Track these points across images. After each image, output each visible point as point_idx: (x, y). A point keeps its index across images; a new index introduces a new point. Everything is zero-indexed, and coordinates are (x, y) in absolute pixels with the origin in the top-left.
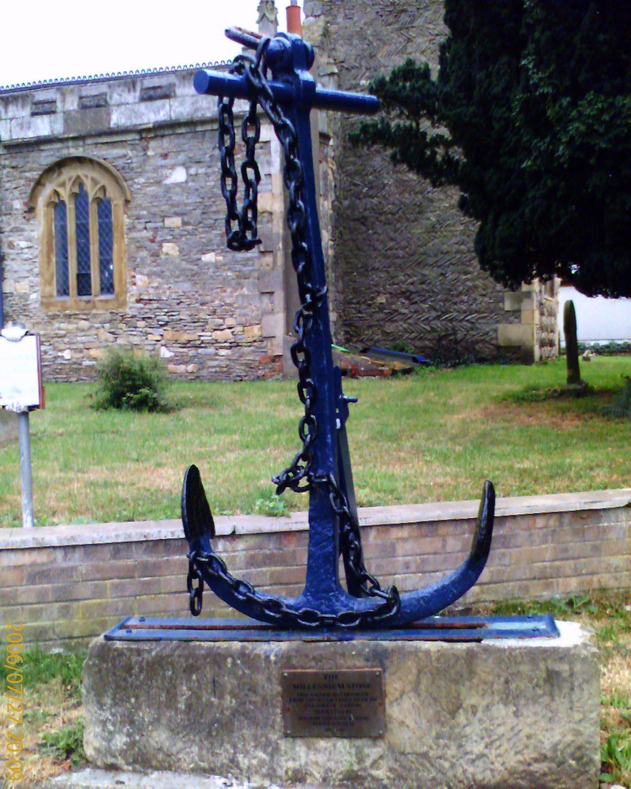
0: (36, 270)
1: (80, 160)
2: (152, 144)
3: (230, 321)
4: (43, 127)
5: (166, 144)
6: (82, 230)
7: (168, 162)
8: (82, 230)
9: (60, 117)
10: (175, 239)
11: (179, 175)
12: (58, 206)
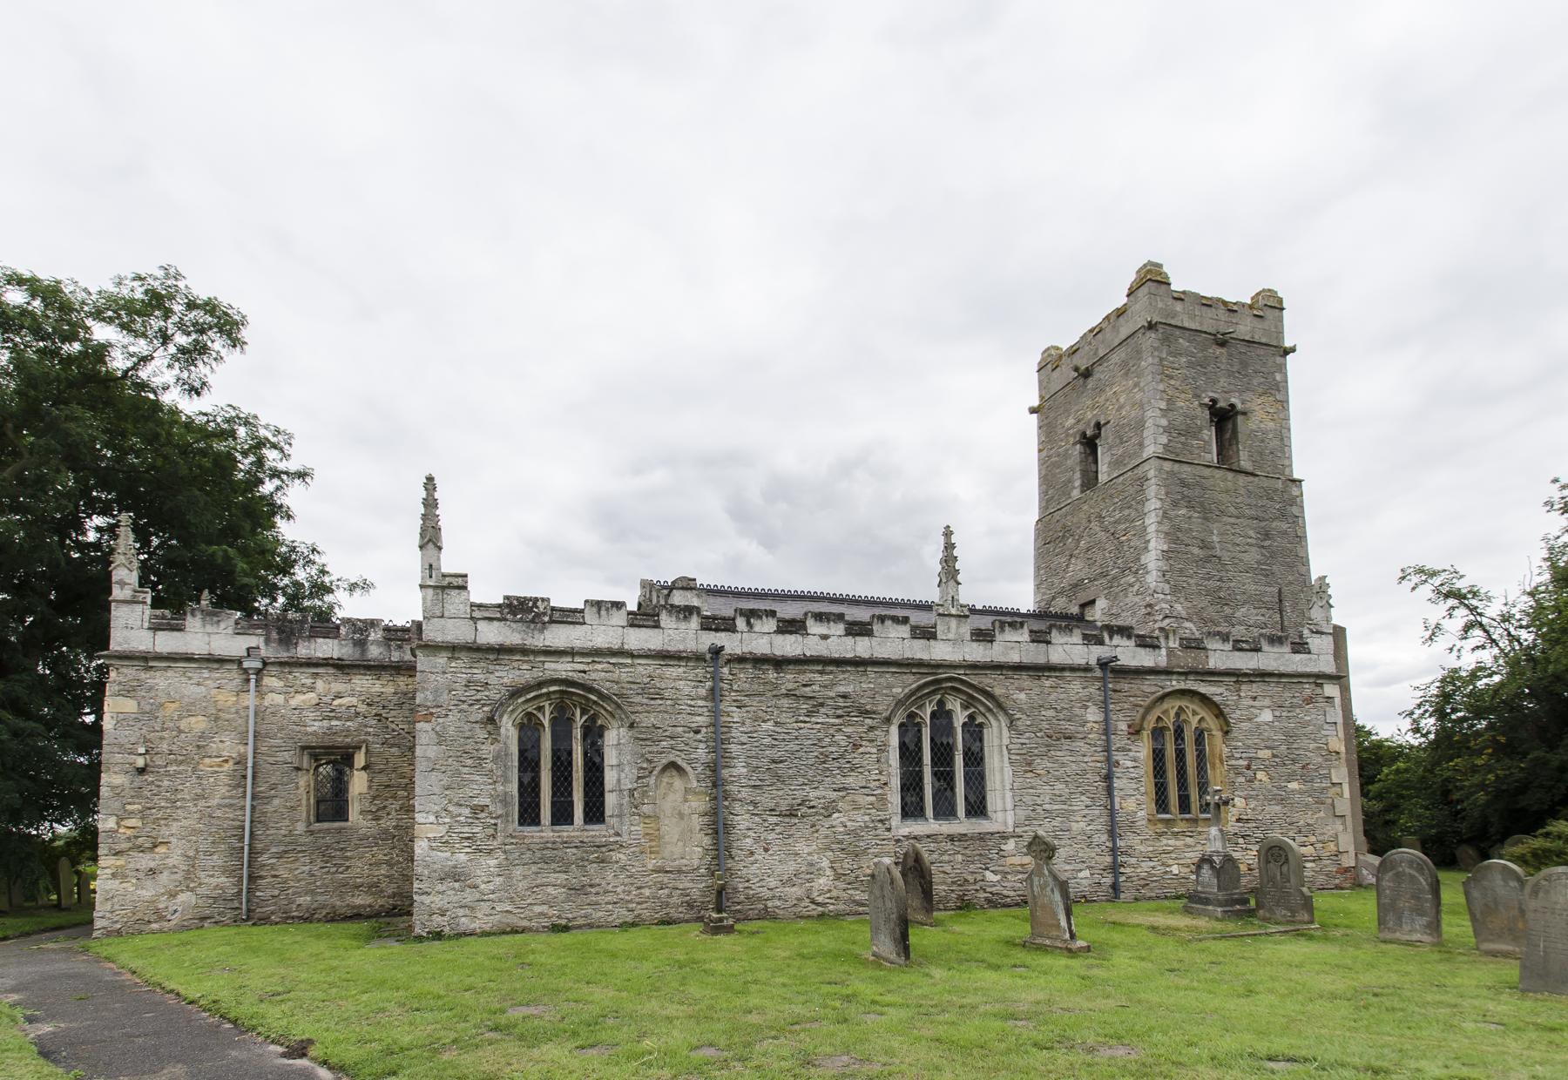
0: (1142, 789)
1: (1205, 699)
2: (1244, 687)
3: (1313, 839)
4: (1146, 659)
5: (1256, 688)
6: (1180, 754)
7: (1256, 703)
8: (1180, 754)
9: (1164, 652)
10: (1266, 769)
11: (1267, 716)
12: (1158, 733)
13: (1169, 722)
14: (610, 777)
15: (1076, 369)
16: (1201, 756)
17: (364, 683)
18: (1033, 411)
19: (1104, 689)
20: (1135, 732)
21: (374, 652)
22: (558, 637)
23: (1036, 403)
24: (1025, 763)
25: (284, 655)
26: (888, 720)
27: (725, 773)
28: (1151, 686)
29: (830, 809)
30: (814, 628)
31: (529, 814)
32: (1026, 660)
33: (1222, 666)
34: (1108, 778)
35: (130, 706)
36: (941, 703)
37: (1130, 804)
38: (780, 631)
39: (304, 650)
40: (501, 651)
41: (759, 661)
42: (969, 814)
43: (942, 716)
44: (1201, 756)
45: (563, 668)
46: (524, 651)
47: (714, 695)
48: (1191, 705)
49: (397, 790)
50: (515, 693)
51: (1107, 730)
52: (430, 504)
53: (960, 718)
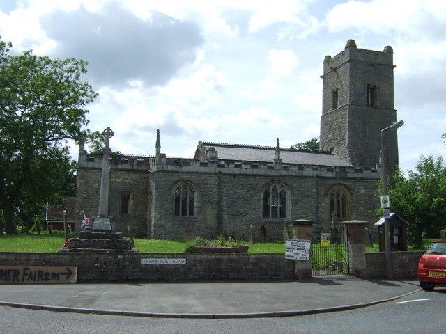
4: (330, 174)
6: (338, 201)
11: (363, 191)
13: (335, 192)
14: (195, 204)
15: (331, 68)
16: (344, 201)
17: (133, 176)
18: (321, 77)
19: (317, 183)
20: (326, 195)
21: (135, 167)
22: (185, 169)
23: (322, 74)
24: (295, 203)
25: (115, 168)
26: (261, 191)
27: (221, 204)
28: (330, 182)
29: (246, 214)
30: (244, 166)
31: (177, 213)
32: (298, 175)
33: (351, 176)
34: (317, 208)
35: (82, 181)
36: (275, 186)
37: (323, 216)
38: (235, 167)
39: (120, 167)
40: (173, 172)
41: (230, 175)
42: (281, 217)
43: (275, 189)
44: (344, 201)
45: (186, 176)
46: (177, 172)
47: (219, 184)
48: (342, 188)
49: (145, 206)
50: (176, 183)
51: (318, 194)
52: (158, 136)
53: (279, 191)
